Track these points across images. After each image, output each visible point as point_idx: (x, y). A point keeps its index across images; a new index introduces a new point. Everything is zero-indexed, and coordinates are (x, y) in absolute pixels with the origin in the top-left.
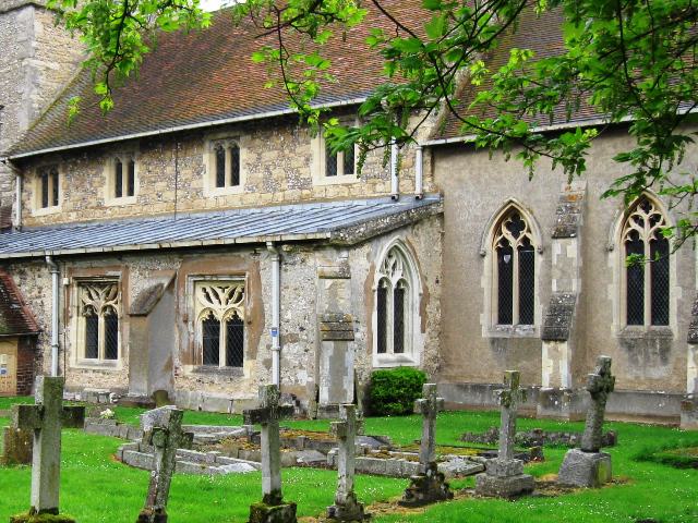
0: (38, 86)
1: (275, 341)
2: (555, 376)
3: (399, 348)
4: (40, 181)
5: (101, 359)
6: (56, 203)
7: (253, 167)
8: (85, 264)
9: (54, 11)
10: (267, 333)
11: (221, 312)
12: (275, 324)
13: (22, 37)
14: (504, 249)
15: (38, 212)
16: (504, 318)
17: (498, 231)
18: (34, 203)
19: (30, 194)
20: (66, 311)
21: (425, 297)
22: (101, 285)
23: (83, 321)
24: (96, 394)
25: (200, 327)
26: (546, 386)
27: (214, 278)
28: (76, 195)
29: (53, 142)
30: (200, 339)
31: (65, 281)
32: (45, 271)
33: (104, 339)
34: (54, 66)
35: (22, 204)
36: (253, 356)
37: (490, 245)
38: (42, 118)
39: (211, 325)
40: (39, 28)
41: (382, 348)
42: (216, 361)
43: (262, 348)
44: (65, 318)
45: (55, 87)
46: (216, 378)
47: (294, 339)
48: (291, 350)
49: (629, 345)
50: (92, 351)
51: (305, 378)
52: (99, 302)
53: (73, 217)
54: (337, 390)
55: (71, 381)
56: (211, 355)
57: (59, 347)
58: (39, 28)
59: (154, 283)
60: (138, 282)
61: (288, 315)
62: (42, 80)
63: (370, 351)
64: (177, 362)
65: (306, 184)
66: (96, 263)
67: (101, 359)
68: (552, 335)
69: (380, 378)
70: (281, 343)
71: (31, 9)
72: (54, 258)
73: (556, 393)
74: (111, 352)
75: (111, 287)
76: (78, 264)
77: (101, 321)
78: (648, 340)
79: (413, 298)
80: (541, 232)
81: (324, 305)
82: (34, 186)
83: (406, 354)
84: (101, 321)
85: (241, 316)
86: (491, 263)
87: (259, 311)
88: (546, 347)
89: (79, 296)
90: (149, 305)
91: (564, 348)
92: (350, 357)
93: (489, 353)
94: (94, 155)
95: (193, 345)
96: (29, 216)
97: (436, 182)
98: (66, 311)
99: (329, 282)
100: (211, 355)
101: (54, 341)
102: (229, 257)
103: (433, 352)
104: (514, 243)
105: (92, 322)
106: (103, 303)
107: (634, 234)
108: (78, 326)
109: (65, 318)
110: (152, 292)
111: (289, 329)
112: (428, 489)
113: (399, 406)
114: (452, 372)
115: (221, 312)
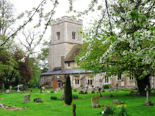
0: (67, 52)
1: (95, 82)
2: (123, 85)
3: (108, 82)
4: (68, 64)
5: (77, 84)
6: (70, 66)
8: (75, 74)
9: (52, 14)
10: (94, 81)
11: (90, 79)
12: (95, 80)
13: (65, 46)
15: (68, 68)
18: (67, 66)
19: (67, 65)
20: (73, 79)
22: (77, 77)
23: (75, 80)
24: (77, 88)
25: (88, 81)
26: (122, 86)
27: (89, 76)
28: (72, 66)
29: (69, 59)
30: (88, 82)
31: (73, 76)
32: (71, 75)
33: (77, 82)
34: (69, 49)
35: (66, 66)
36: (93, 83)
38: (67, 56)
39: (89, 80)
40: (67, 45)
41: (106, 82)
42: (89, 84)
43: (94, 83)
44: (73, 80)
45: (69, 52)
46: (89, 86)
47: (97, 82)
48: (96, 83)
49: (130, 82)
50: (76, 83)
51: (98, 85)
52: (77, 78)
54: (101, 86)
55: (74, 87)
56: (89, 84)
57: (72, 83)
58: (67, 45)
59: (83, 76)
61: (96, 79)
62: (67, 51)
63: (104, 83)
64: (85, 84)
66: (76, 74)
67: (77, 84)
68: (122, 81)
69: (106, 85)
70: (96, 82)
71: (66, 43)
72: (72, 74)
73: (123, 86)
74: (78, 83)
75: (78, 77)
76: (74, 74)
77: (77, 80)
78: (132, 81)
81: (100, 79)
82: (67, 64)
83: (109, 83)
84: (77, 80)
85: (92, 80)
87: (93, 79)
88: (122, 82)
89: (74, 78)
90: (82, 79)
91: (123, 82)
92: (102, 83)
95: (87, 83)
96: (67, 68)
98: (73, 79)
99: (100, 76)
101: (72, 83)
102: (90, 74)
103: (111, 83)
105: (76, 80)
106: (77, 78)
108: (74, 81)
109: (73, 80)
110: (82, 77)
111: (96, 81)
113: (107, 88)
114: (114, 85)
115: (90, 79)
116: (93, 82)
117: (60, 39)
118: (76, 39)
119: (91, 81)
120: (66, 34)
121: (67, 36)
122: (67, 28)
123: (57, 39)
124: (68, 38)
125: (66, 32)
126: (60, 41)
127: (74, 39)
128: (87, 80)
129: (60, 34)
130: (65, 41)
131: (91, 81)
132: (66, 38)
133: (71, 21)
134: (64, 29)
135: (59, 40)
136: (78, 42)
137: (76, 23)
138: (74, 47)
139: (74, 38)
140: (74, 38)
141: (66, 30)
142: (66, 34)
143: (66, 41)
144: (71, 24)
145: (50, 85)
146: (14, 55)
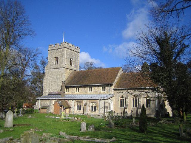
6: (68, 92)
7: (94, 90)
11: (94, 106)
14: (121, 100)
16: (121, 106)
17: (120, 98)
21: (113, 104)
37: (120, 99)
39: (92, 107)
44: (75, 106)
52: (79, 104)
53: (71, 94)
60: (84, 102)
65: (100, 92)
79: (112, 104)
80: (162, 141)
86: (120, 101)
93: (119, 110)
94: (74, 87)
97: (83, 67)
100: (92, 110)
104: (122, 99)
105: (78, 106)
107: (133, 99)
112: (190, 32)
116: (97, 109)
117: (57, 64)
118: (73, 66)
119: (95, 107)
120: (65, 60)
121: (65, 61)
122: (66, 54)
123: (55, 64)
124: (66, 64)
125: (66, 58)
126: (58, 66)
127: (72, 65)
128: (91, 106)
129: (58, 59)
130: (63, 67)
131: (95, 107)
132: (65, 63)
133: (70, 48)
134: (63, 55)
135: (57, 65)
136: (75, 69)
137: (74, 50)
138: (71, 74)
139: (71, 64)
140: (71, 64)
141: (66, 56)
142: (65, 60)
143: (65, 67)
144: (70, 50)
145: (48, 109)
146: (18, 113)
